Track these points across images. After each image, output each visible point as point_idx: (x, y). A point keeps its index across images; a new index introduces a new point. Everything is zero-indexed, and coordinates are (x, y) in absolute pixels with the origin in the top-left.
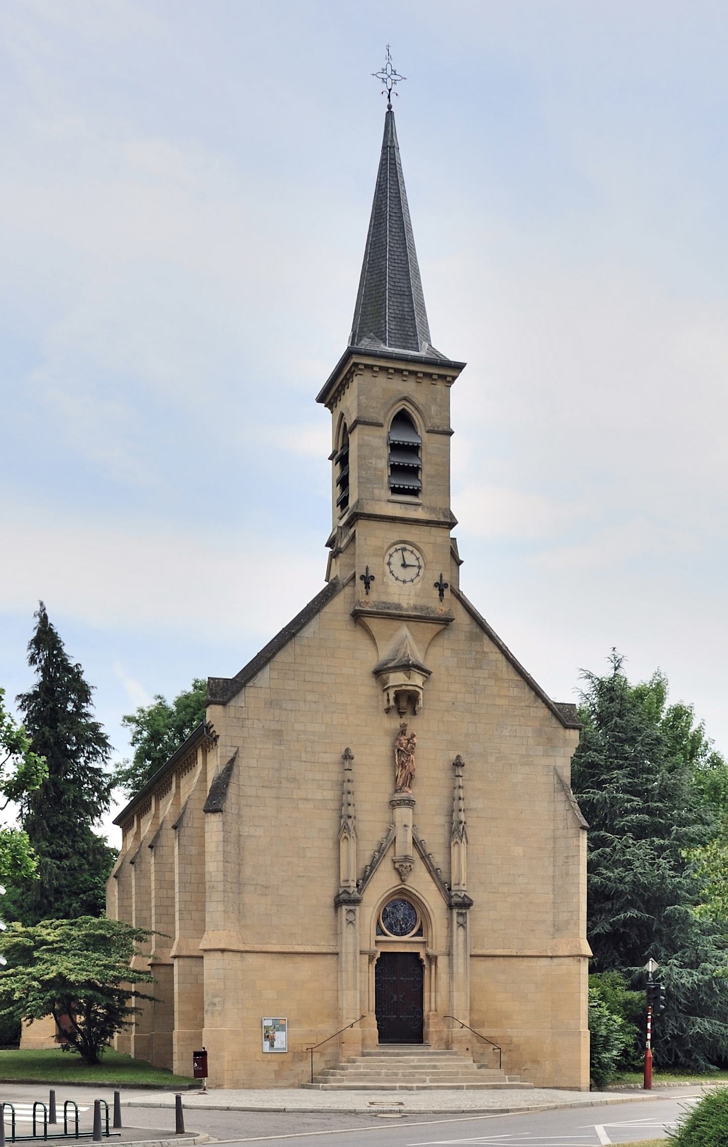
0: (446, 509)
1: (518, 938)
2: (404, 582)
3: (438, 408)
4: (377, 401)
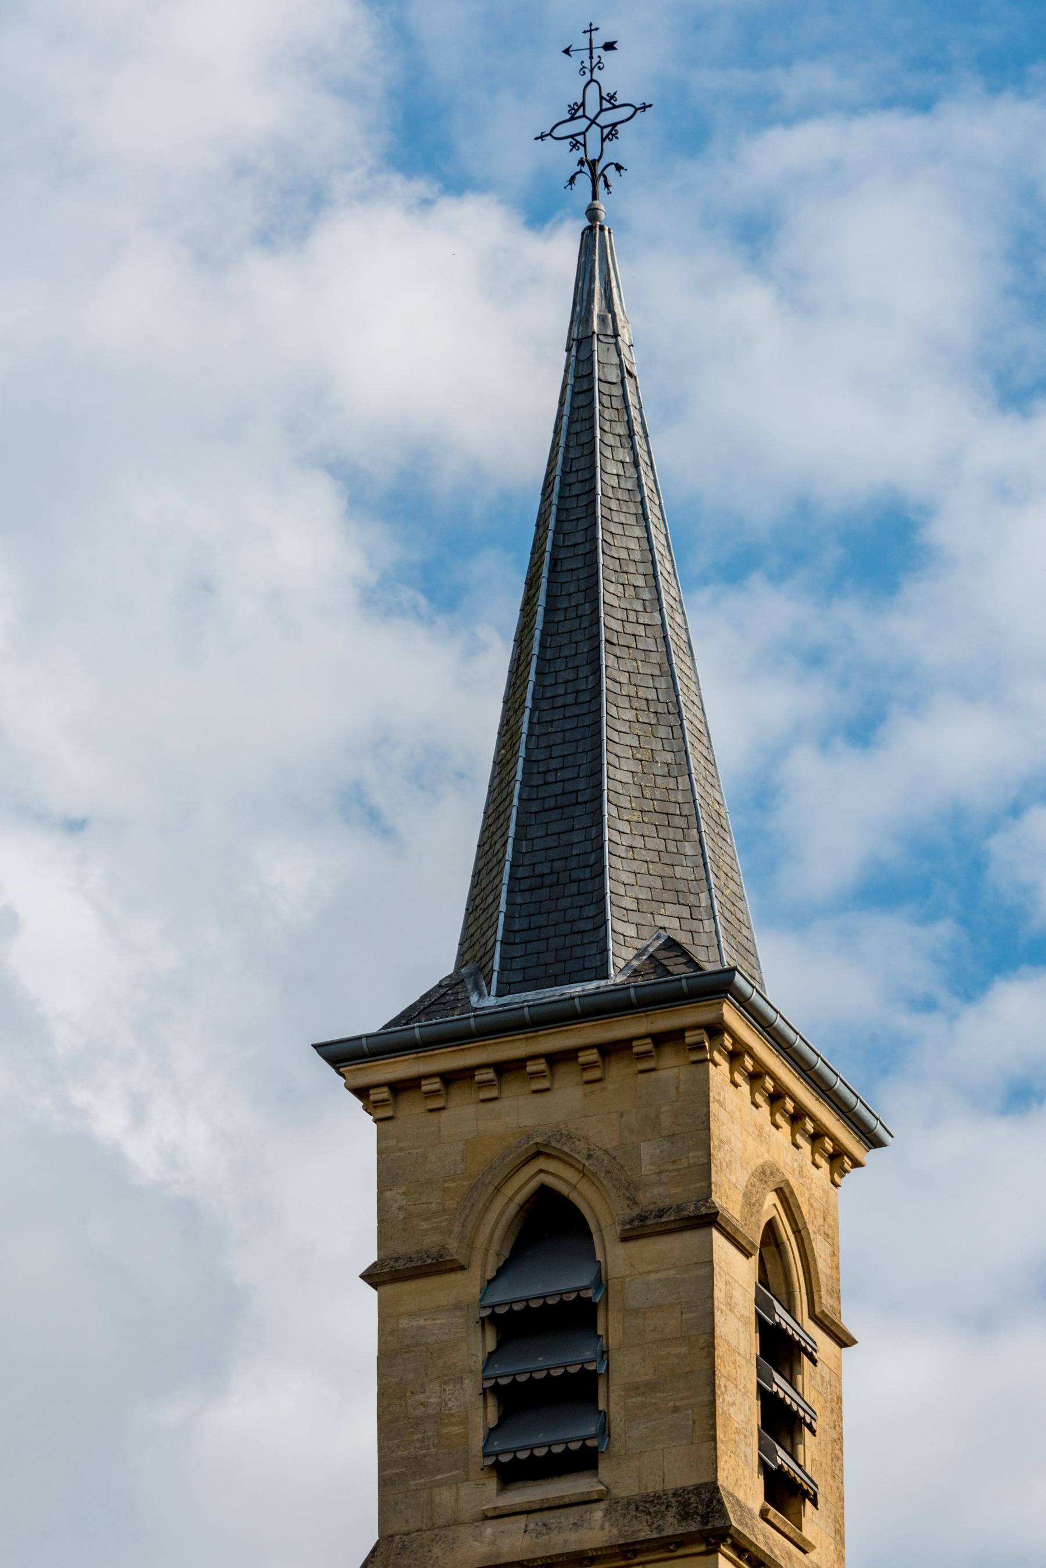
0: (697, 1489)
3: (667, 1146)
4: (445, 1190)
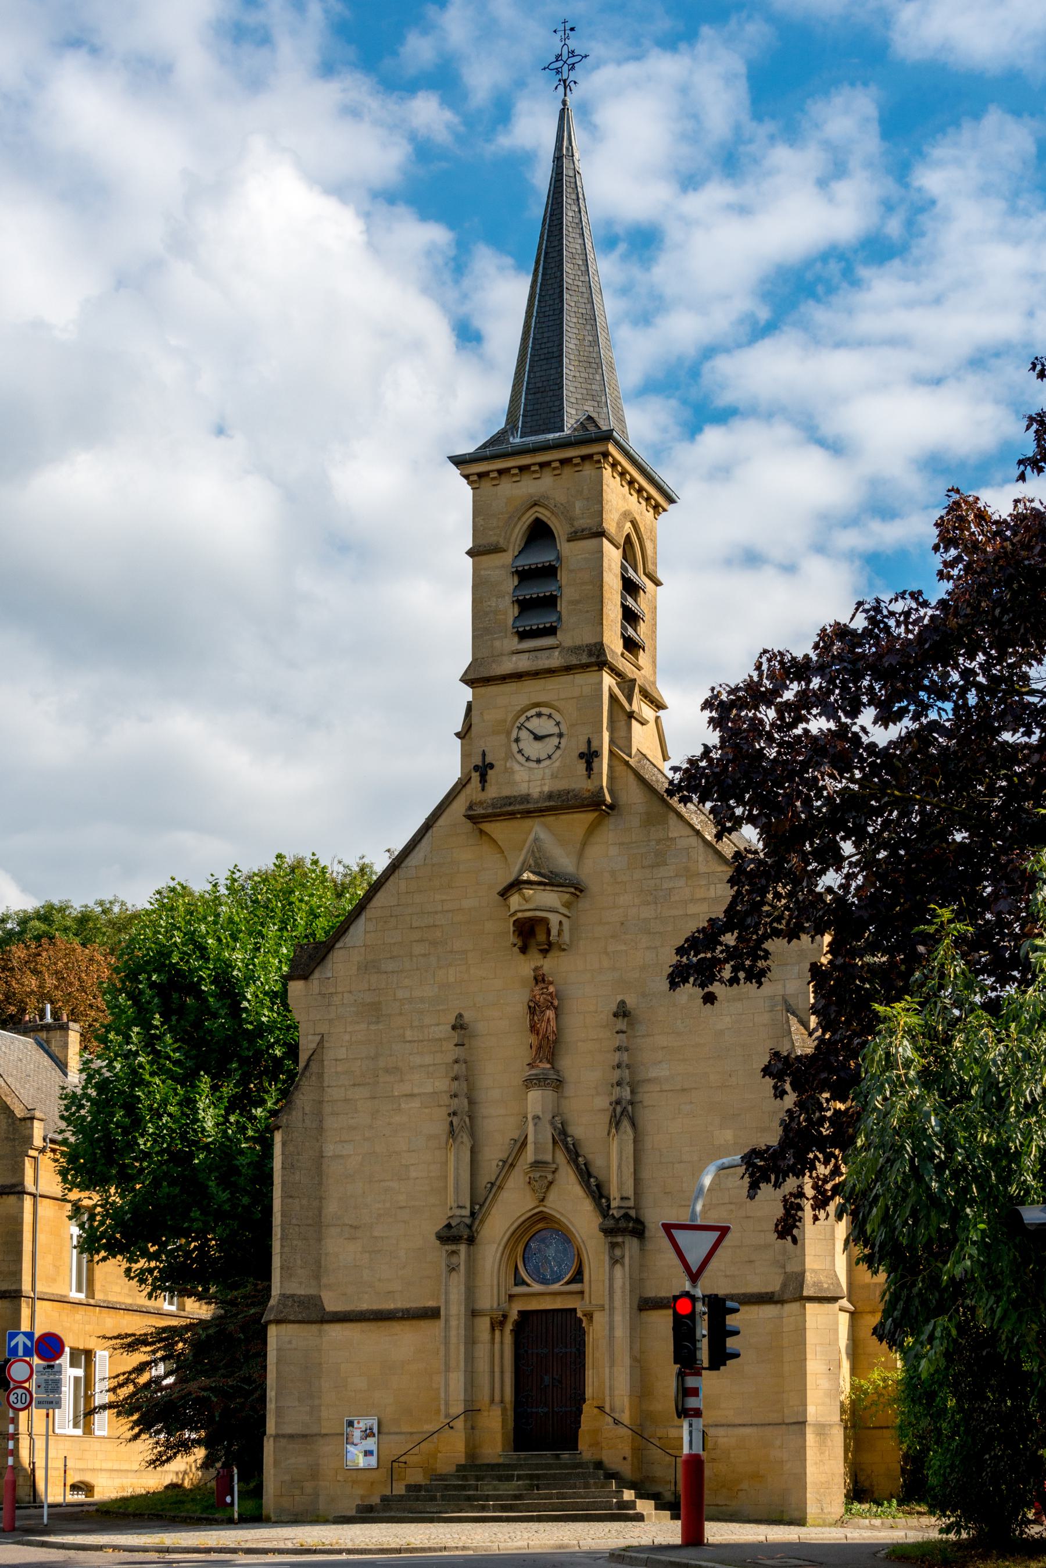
1: (726, 1276)
2: (539, 761)
